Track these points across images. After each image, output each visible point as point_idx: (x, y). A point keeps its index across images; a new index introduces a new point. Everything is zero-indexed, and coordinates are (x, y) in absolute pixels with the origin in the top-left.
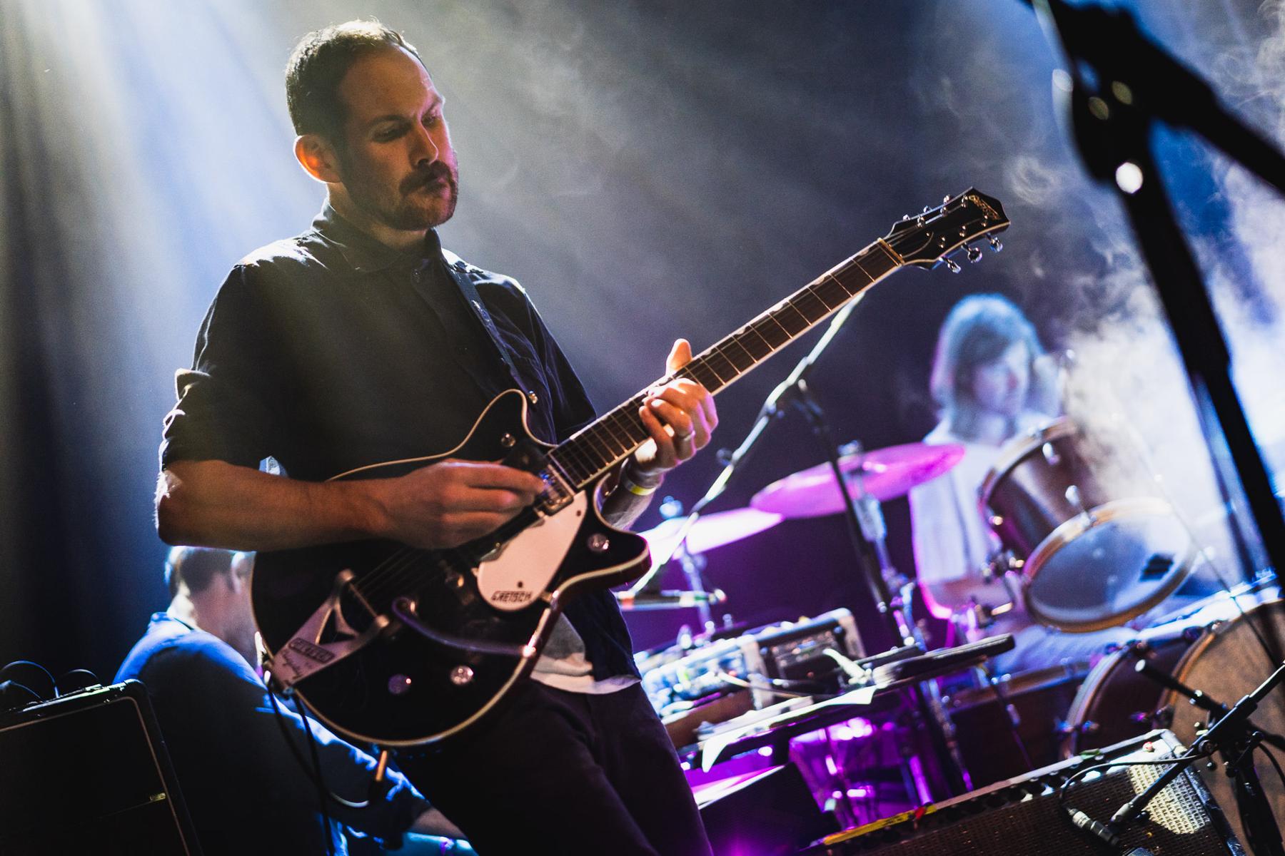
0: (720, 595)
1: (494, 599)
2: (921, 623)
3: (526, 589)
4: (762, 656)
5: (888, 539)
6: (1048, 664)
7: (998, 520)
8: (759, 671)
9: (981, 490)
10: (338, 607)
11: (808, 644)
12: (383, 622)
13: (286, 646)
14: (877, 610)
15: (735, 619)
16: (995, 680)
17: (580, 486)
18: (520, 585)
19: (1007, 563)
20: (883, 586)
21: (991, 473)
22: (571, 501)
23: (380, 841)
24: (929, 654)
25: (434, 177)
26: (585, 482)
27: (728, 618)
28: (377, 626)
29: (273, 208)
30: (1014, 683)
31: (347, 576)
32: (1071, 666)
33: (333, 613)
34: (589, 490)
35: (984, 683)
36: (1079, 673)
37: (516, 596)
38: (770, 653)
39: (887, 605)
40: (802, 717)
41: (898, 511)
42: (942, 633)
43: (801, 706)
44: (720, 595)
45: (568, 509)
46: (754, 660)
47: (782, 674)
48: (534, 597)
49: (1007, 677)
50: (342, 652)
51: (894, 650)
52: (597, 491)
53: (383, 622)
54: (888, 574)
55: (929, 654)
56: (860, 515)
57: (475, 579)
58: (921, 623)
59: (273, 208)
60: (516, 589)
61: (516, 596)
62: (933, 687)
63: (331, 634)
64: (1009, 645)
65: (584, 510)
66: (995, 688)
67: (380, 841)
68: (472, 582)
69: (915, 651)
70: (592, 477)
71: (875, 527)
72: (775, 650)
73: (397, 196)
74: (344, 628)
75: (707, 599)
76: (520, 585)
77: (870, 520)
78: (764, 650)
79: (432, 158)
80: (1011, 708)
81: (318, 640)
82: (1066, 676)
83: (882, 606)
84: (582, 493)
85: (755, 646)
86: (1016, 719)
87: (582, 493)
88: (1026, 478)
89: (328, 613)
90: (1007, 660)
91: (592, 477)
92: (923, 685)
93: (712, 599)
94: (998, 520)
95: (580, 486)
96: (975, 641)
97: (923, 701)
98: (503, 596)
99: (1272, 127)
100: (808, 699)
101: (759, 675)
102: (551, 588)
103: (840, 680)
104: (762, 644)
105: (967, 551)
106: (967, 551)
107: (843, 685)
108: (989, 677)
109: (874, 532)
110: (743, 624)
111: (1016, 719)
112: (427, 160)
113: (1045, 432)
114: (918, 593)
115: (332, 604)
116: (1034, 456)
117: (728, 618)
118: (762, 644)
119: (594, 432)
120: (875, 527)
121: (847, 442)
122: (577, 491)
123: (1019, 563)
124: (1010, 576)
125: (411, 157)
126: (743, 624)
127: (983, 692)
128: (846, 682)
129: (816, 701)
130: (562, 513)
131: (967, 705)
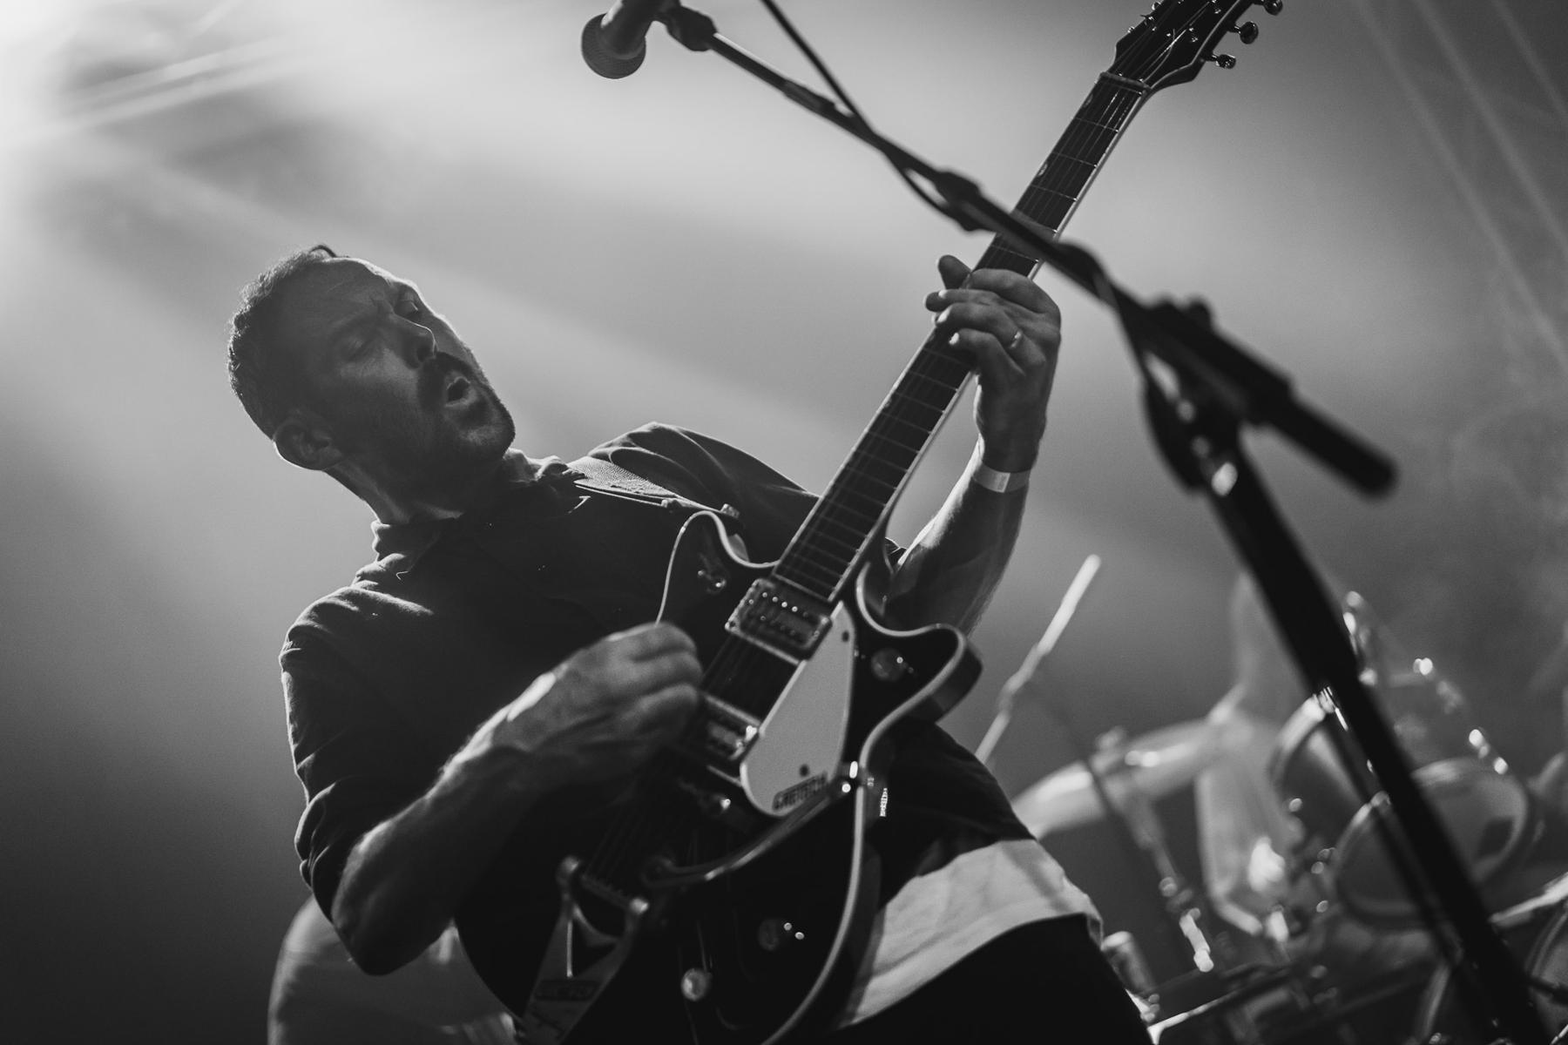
1: (777, 806)
2: (1197, 911)
3: (815, 772)
10: (578, 913)
12: (641, 906)
13: (532, 1000)
17: (832, 597)
18: (804, 771)
23: (711, 875)
26: (839, 585)
28: (634, 915)
29: (323, 541)
31: (572, 865)
33: (576, 925)
34: (848, 596)
45: (830, 637)
50: (607, 972)
52: (860, 590)
53: (641, 906)
57: (741, 791)
59: (323, 541)
63: (585, 955)
65: (851, 629)
67: (711, 875)
68: (738, 794)
74: (597, 937)
76: (804, 771)
81: (569, 973)
87: (840, 605)
89: (570, 927)
95: (832, 597)
102: (850, 754)
108: (1522, 770)
115: (570, 914)
121: (1106, 730)
122: (832, 606)
124: (1319, 869)
130: (823, 646)
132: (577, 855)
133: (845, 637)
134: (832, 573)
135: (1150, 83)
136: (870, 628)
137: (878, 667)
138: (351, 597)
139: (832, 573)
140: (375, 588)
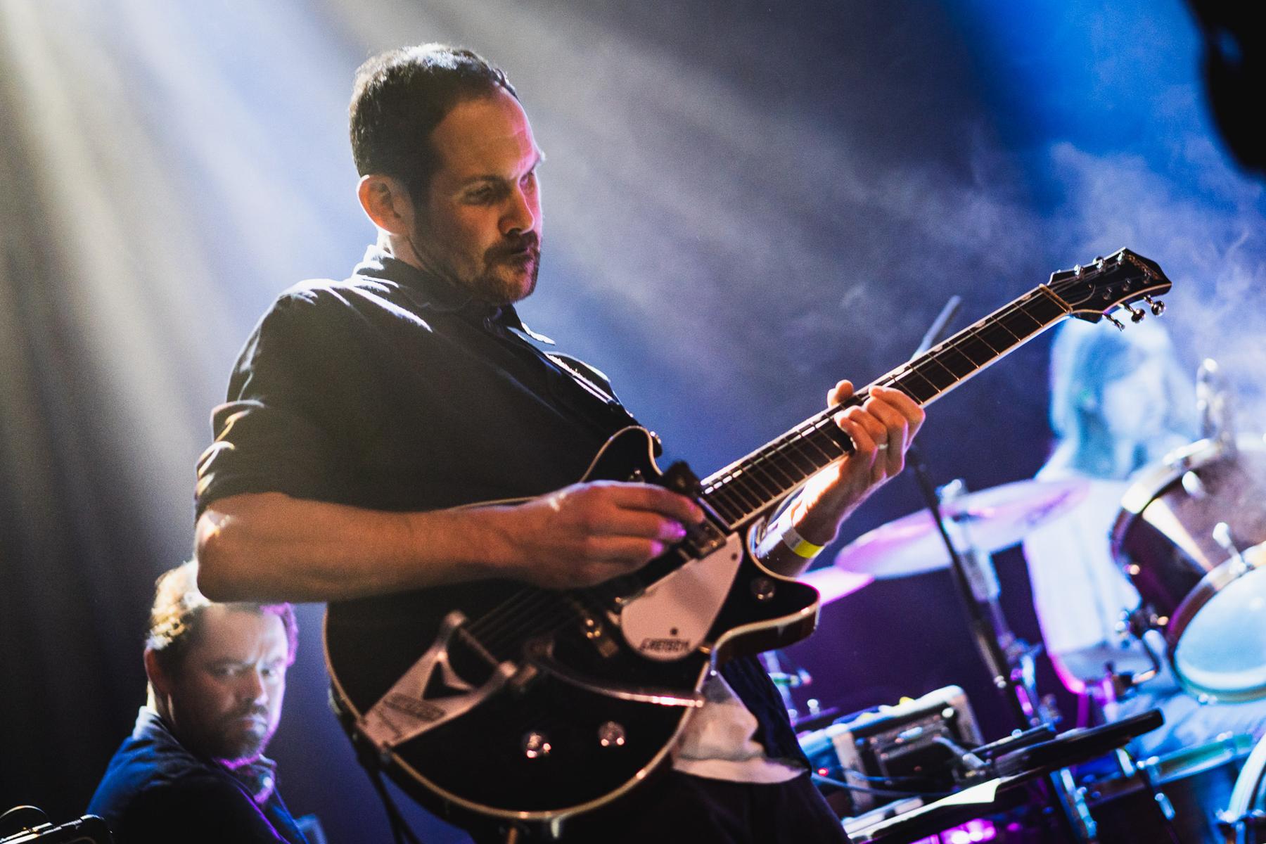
0: (806, 677)
2: (1048, 700)
3: (682, 636)
4: (858, 747)
5: (1002, 598)
6: (1199, 744)
7: (1134, 569)
8: (854, 768)
9: (1113, 536)
11: (913, 732)
14: (995, 686)
15: (822, 705)
16: (1141, 764)
17: (733, 526)
18: (674, 632)
19: (1148, 620)
20: (999, 654)
21: (1123, 514)
22: (723, 544)
24: (1060, 737)
25: (519, 246)
26: (742, 521)
27: (813, 704)
28: (501, 675)
30: (1165, 767)
32: (1229, 744)
35: (1128, 768)
36: (1241, 751)
37: (670, 645)
38: (867, 744)
39: (1007, 678)
40: (911, 820)
41: (1012, 563)
42: (1077, 708)
43: (909, 809)
44: (806, 677)
45: (720, 553)
46: (847, 756)
47: (883, 770)
48: (693, 645)
49: (1153, 761)
51: (1017, 734)
54: (1005, 640)
55: (1060, 737)
56: (969, 572)
58: (1048, 700)
60: (669, 637)
61: (670, 645)
62: (1067, 778)
64: (1153, 720)
65: (740, 553)
66: (1142, 774)
68: (615, 633)
69: (1046, 734)
70: (747, 517)
71: (988, 587)
72: (874, 740)
73: (481, 265)
75: (788, 682)
76: (674, 632)
77: (980, 577)
78: (860, 741)
79: (525, 227)
80: (1160, 797)
82: (1226, 756)
83: (1000, 681)
84: (736, 535)
85: (848, 737)
86: (1169, 812)
87: (736, 535)
88: (1163, 518)
90: (1153, 740)
91: (747, 517)
92: (1053, 776)
93: (795, 681)
94: (1134, 569)
95: (733, 526)
96: (1113, 713)
97: (1056, 794)
98: (655, 644)
99: (692, 144)
100: (918, 802)
101: (855, 773)
102: (711, 637)
103: (955, 773)
104: (857, 734)
105: (1100, 610)
106: (1100, 610)
107: (958, 780)
108: (1134, 760)
109: (986, 590)
110: (832, 710)
111: (1169, 812)
112: (519, 230)
113: (1186, 462)
114: (1045, 665)
116: (1173, 489)
117: (813, 704)
118: (857, 734)
119: (749, 475)
120: (988, 587)
122: (728, 533)
123: (1163, 621)
125: (501, 224)
126: (832, 710)
127: (1124, 780)
128: (962, 776)
129: (926, 803)
130: (713, 557)
131: (1110, 797)
132: (464, 611)
133: (734, 557)
134: (750, 505)
135: (1075, 308)
136: (836, 522)
137: (765, 583)
138: (346, 293)
139: (750, 505)
140: (393, 296)
